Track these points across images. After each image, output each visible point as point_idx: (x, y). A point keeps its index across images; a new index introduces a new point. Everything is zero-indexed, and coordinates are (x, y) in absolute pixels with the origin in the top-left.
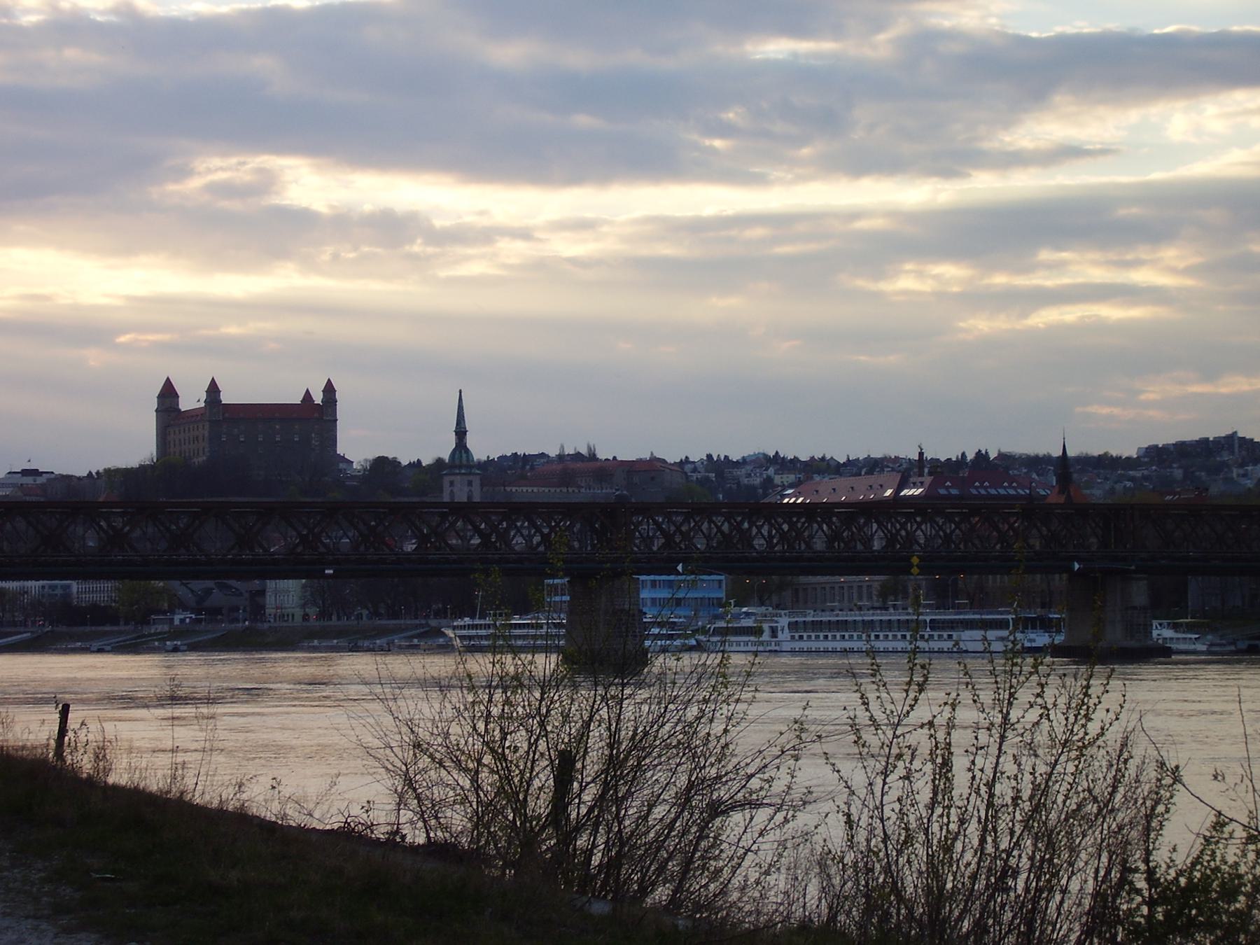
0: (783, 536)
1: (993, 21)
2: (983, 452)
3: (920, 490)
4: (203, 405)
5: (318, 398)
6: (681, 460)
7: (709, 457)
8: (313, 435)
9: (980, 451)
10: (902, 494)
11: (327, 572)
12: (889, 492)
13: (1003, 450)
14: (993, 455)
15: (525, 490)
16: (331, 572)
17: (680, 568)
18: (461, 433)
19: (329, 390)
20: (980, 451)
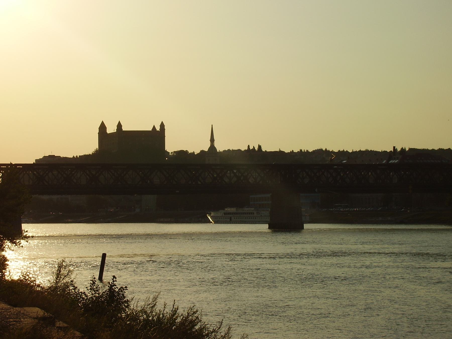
2: (404, 148)
3: (397, 161)
4: (116, 131)
5: (158, 129)
6: (291, 151)
7: (301, 150)
9: (402, 148)
10: (390, 162)
11: (176, 192)
12: (384, 162)
14: (407, 149)
16: (178, 192)
17: (316, 190)
18: (212, 140)
19: (162, 126)
20: (402, 148)
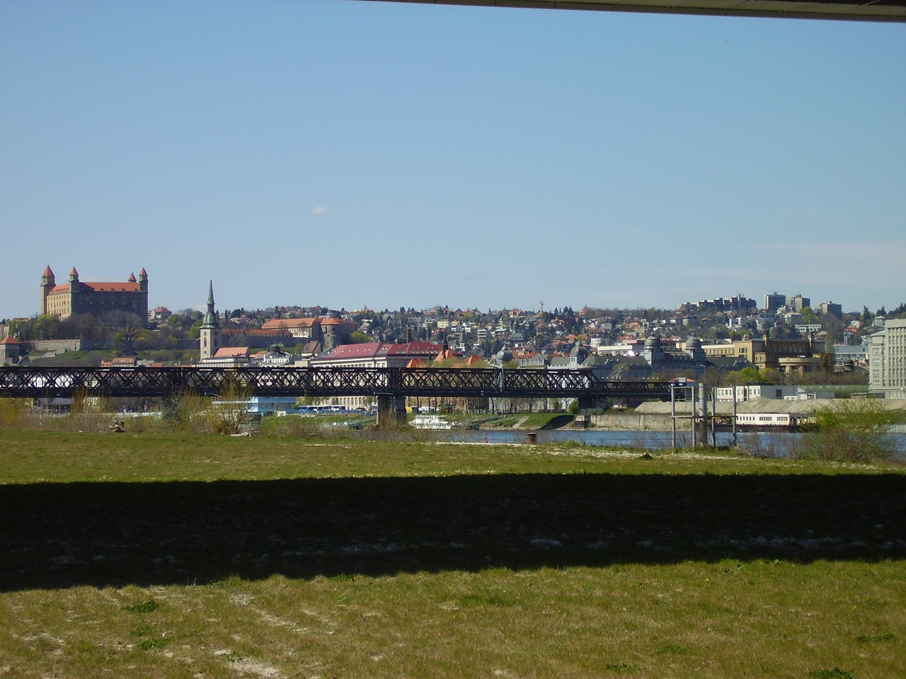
0: (346, 381)
1: (721, 444)
2: (569, 308)
5: (138, 279)
8: (134, 301)
9: (566, 307)
13: (588, 306)
15: (790, 399)
19: (144, 276)
20: (566, 307)
